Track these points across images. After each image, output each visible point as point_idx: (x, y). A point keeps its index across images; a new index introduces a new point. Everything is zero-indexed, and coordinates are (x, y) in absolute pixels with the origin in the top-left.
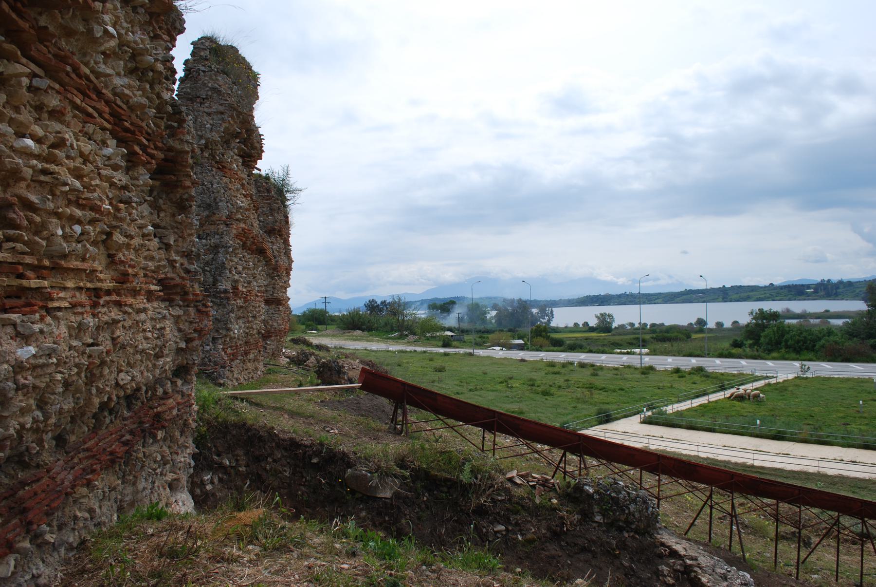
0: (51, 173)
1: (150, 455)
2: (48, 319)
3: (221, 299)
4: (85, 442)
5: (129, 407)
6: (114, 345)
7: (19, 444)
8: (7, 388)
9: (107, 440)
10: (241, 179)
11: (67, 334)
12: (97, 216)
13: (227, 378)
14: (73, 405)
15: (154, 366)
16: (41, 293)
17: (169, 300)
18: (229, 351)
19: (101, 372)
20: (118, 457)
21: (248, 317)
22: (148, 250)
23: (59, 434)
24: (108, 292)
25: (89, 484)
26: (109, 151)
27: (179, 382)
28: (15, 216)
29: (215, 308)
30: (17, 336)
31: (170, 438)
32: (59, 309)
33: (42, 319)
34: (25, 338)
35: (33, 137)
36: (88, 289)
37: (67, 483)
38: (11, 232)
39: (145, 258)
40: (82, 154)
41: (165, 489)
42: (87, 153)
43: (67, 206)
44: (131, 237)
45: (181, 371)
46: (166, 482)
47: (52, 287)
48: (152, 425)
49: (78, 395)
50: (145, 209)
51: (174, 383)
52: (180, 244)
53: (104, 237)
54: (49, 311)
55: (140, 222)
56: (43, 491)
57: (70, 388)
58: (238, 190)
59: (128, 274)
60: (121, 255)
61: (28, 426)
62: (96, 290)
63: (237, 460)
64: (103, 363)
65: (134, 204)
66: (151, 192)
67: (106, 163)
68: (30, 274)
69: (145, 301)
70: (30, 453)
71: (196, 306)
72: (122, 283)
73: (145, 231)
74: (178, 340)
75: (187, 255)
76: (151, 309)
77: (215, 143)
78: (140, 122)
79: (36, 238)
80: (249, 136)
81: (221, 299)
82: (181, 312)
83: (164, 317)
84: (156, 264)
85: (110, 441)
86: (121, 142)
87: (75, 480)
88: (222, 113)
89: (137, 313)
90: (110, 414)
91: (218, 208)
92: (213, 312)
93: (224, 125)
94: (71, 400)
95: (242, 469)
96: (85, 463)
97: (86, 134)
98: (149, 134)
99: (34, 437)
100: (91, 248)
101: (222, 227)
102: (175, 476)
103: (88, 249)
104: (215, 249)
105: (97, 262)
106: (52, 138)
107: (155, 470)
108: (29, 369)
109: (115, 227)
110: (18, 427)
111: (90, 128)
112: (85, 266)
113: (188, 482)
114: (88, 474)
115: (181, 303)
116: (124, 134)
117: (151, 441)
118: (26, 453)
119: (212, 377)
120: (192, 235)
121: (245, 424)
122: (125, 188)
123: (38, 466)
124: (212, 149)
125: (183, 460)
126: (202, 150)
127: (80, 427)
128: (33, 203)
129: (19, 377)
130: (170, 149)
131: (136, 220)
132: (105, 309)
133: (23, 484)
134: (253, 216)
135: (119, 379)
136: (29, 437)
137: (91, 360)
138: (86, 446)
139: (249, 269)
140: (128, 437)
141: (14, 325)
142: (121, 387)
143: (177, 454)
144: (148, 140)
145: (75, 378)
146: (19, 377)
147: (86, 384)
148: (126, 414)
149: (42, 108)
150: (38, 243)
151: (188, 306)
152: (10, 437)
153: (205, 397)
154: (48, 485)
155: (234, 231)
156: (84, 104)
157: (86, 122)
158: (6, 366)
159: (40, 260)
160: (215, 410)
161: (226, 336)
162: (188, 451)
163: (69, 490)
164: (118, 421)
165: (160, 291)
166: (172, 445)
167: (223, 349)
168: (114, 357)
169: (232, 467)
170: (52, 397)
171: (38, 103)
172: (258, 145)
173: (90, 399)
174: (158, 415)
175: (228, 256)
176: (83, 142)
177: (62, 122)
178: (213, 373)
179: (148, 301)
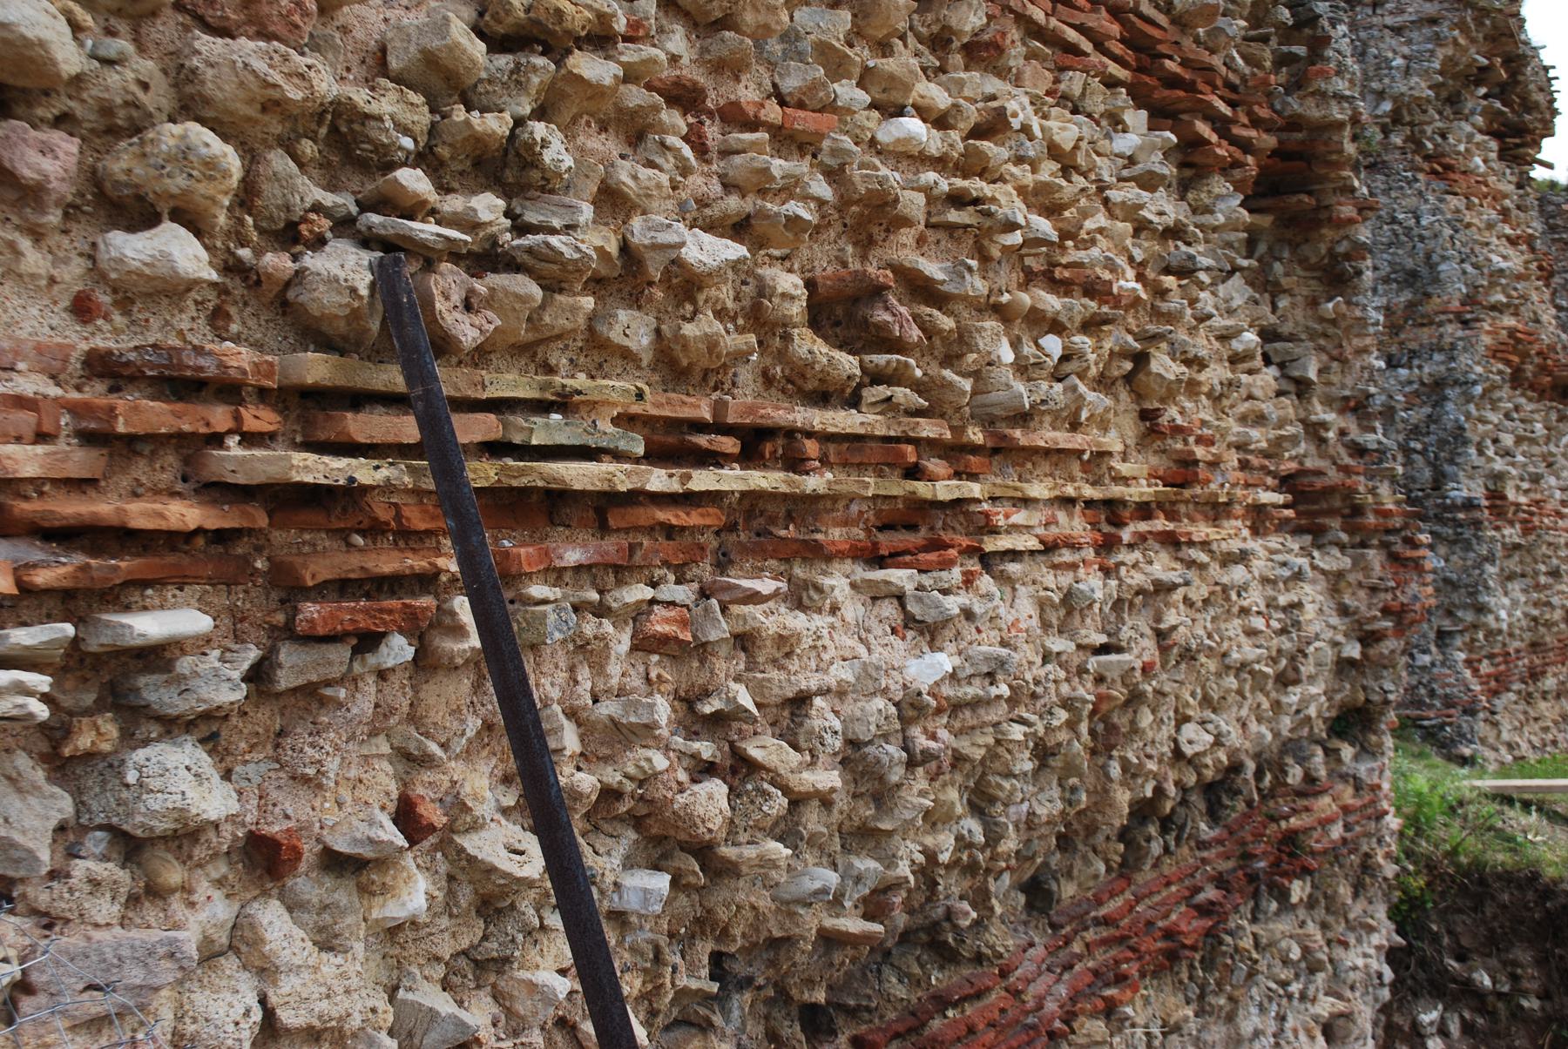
0: (976, 201)
1: (1272, 944)
2: (986, 582)
3: (1457, 526)
4: (1099, 903)
5: (1213, 815)
6: (1164, 650)
7: (929, 900)
8: (885, 759)
9: (1157, 898)
10: (1498, 196)
11: (1035, 622)
12: (1105, 309)
13: (1483, 741)
14: (1060, 805)
15: (1277, 706)
16: (967, 514)
17: (1311, 529)
18: (1485, 668)
19: (1133, 722)
20: (1184, 946)
21: (1536, 573)
22: (1250, 397)
23: (1034, 878)
24: (1144, 511)
25: (1109, 1011)
26: (1126, 143)
27: (1347, 752)
28: (888, 317)
29: (1442, 550)
30: (906, 627)
31: (1323, 900)
32: (1014, 555)
33: (969, 580)
34: (930, 632)
35: (923, 112)
36: (1089, 503)
37: (1051, 1006)
38: (881, 359)
39: (1243, 419)
40: (1054, 151)
41: (1312, 1038)
42: (1068, 146)
43: (1024, 286)
44: (1197, 363)
45: (1352, 722)
46: (1316, 1018)
47: (993, 499)
48: (1276, 864)
49: (1073, 781)
50: (1237, 290)
51: (1331, 754)
52: (1335, 378)
53: (1128, 366)
54: (987, 561)
55: (1219, 322)
56: (991, 1025)
57: (1053, 762)
58: (1490, 226)
59: (1196, 462)
60: (1173, 412)
61: (944, 857)
62: (1110, 504)
63: (1514, 978)
64: (1135, 698)
65: (1204, 277)
66: (1250, 247)
67: (1125, 173)
68: (935, 465)
69: (1246, 532)
70: (955, 927)
71: (1385, 545)
72: (1182, 486)
73: (1237, 345)
74: (1340, 638)
75: (1357, 406)
76: (1262, 553)
77: (1421, 104)
78: (1205, 56)
79: (948, 373)
80: (1514, 74)
81: (1457, 526)
82: (1346, 562)
83: (1298, 576)
84: (1273, 434)
85: (1163, 903)
86: (1160, 116)
87: (1073, 999)
88: (1433, 21)
89: (1224, 564)
90: (1164, 830)
91: (1436, 280)
92: (1433, 561)
93: (1441, 53)
94: (1056, 792)
95: (1530, 1004)
96: (1101, 957)
97: (1064, 99)
98: (1232, 87)
99: (966, 883)
100: (1091, 396)
101: (1452, 331)
102: (1341, 1006)
103: (1081, 397)
104: (1435, 390)
105: (1113, 433)
106: (973, 114)
107: (1284, 984)
108: (939, 711)
109: (1155, 338)
110: (920, 858)
111: (1074, 82)
112: (1077, 441)
113: (1375, 1024)
114: (1107, 985)
115: (1344, 537)
116: (1166, 93)
117: (1274, 905)
118: (946, 925)
119: (1438, 736)
120: (1365, 351)
121: (1535, 876)
122: (1175, 232)
123: (979, 958)
124: (1411, 124)
125: (1360, 962)
126: (1386, 131)
127: (1086, 861)
128: (929, 281)
129: (916, 732)
130: (1295, 123)
131: (1209, 317)
132: (1137, 555)
133: (942, 1002)
134: (1538, 298)
135: (1182, 739)
136: (952, 886)
137: (1103, 689)
138: (1103, 911)
139: (1533, 441)
140: (1210, 893)
141: (900, 598)
142: (1190, 762)
143: (1345, 945)
144: (1231, 104)
145: (1063, 736)
146: (916, 732)
147: (1093, 752)
148: (1205, 830)
149: (950, 41)
150: (950, 385)
151: (1363, 545)
152: (899, 883)
153: (1419, 794)
154: (1002, 1011)
155: (1487, 340)
156: (1054, 22)
157: (1062, 69)
158: (879, 703)
159: (958, 430)
160: (1449, 833)
161: (1475, 627)
162: (1376, 939)
163: (1058, 1024)
164: (1185, 850)
165: (1286, 506)
166: (1330, 919)
167: (1469, 662)
168: (1163, 680)
169: (1500, 995)
170: (1007, 785)
171: (935, 29)
172: (1540, 98)
173: (1106, 791)
174: (1291, 840)
175: (1472, 408)
176: (1057, 118)
177: (1002, 73)
178: (1442, 727)
179: (1255, 531)
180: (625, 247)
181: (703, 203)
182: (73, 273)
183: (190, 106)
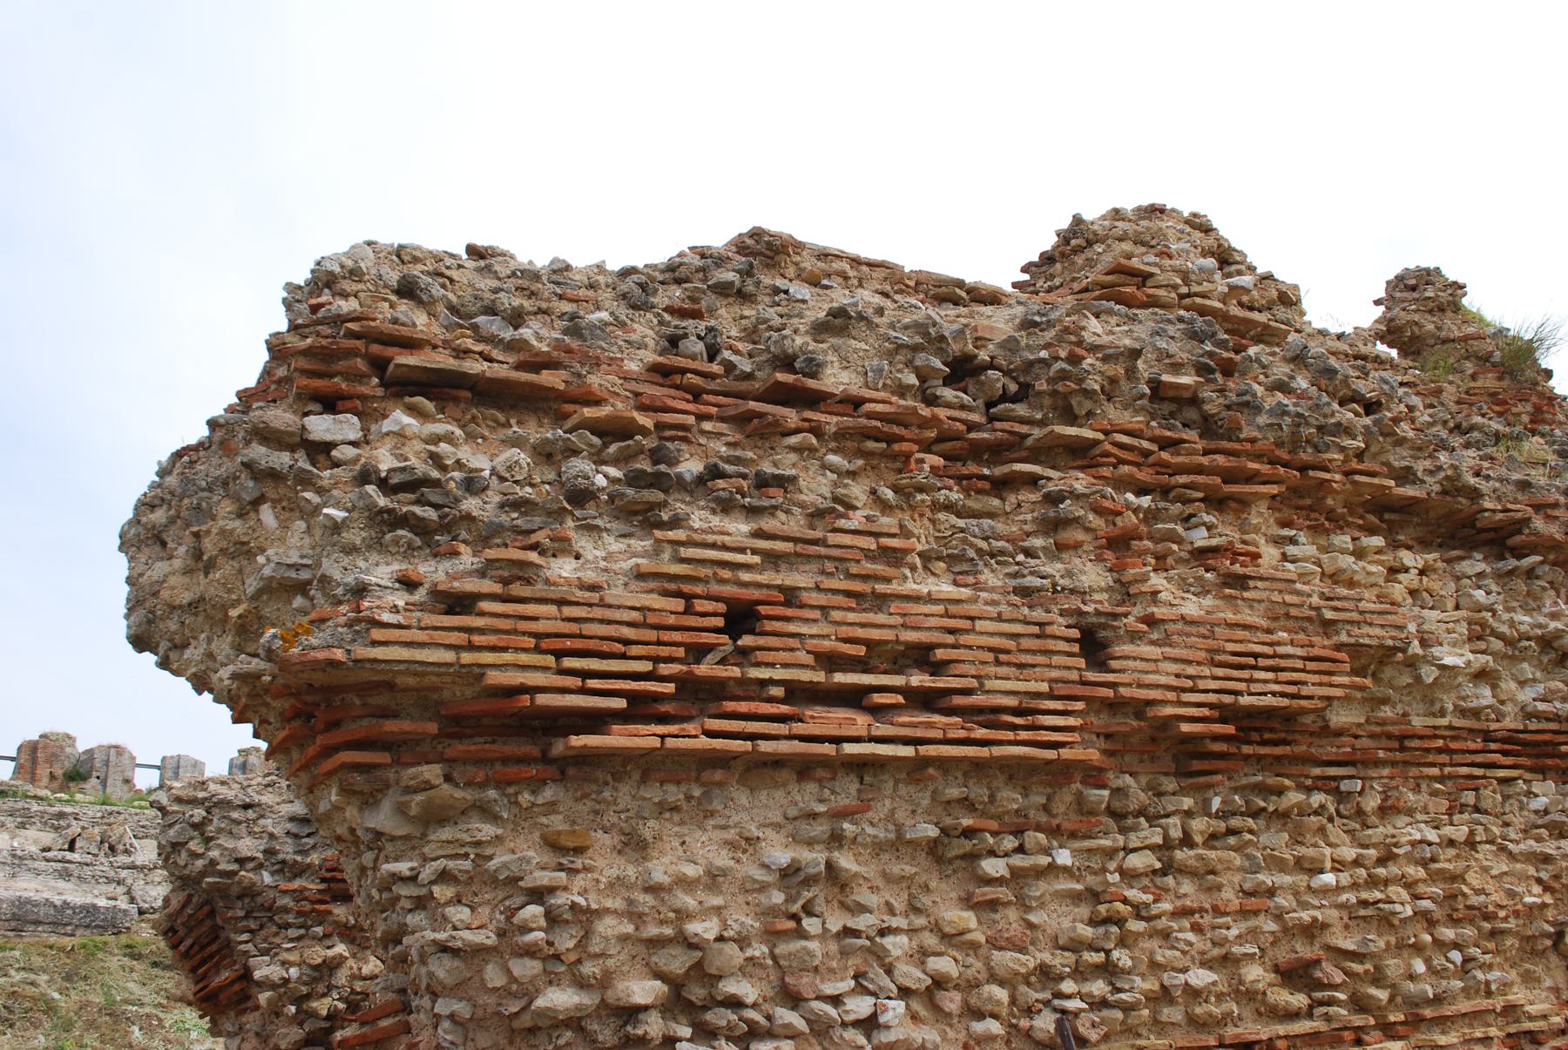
38: (1318, 995)
180: (1162, 985)
181: (1203, 953)
182: (962, 1036)
183: (994, 978)
